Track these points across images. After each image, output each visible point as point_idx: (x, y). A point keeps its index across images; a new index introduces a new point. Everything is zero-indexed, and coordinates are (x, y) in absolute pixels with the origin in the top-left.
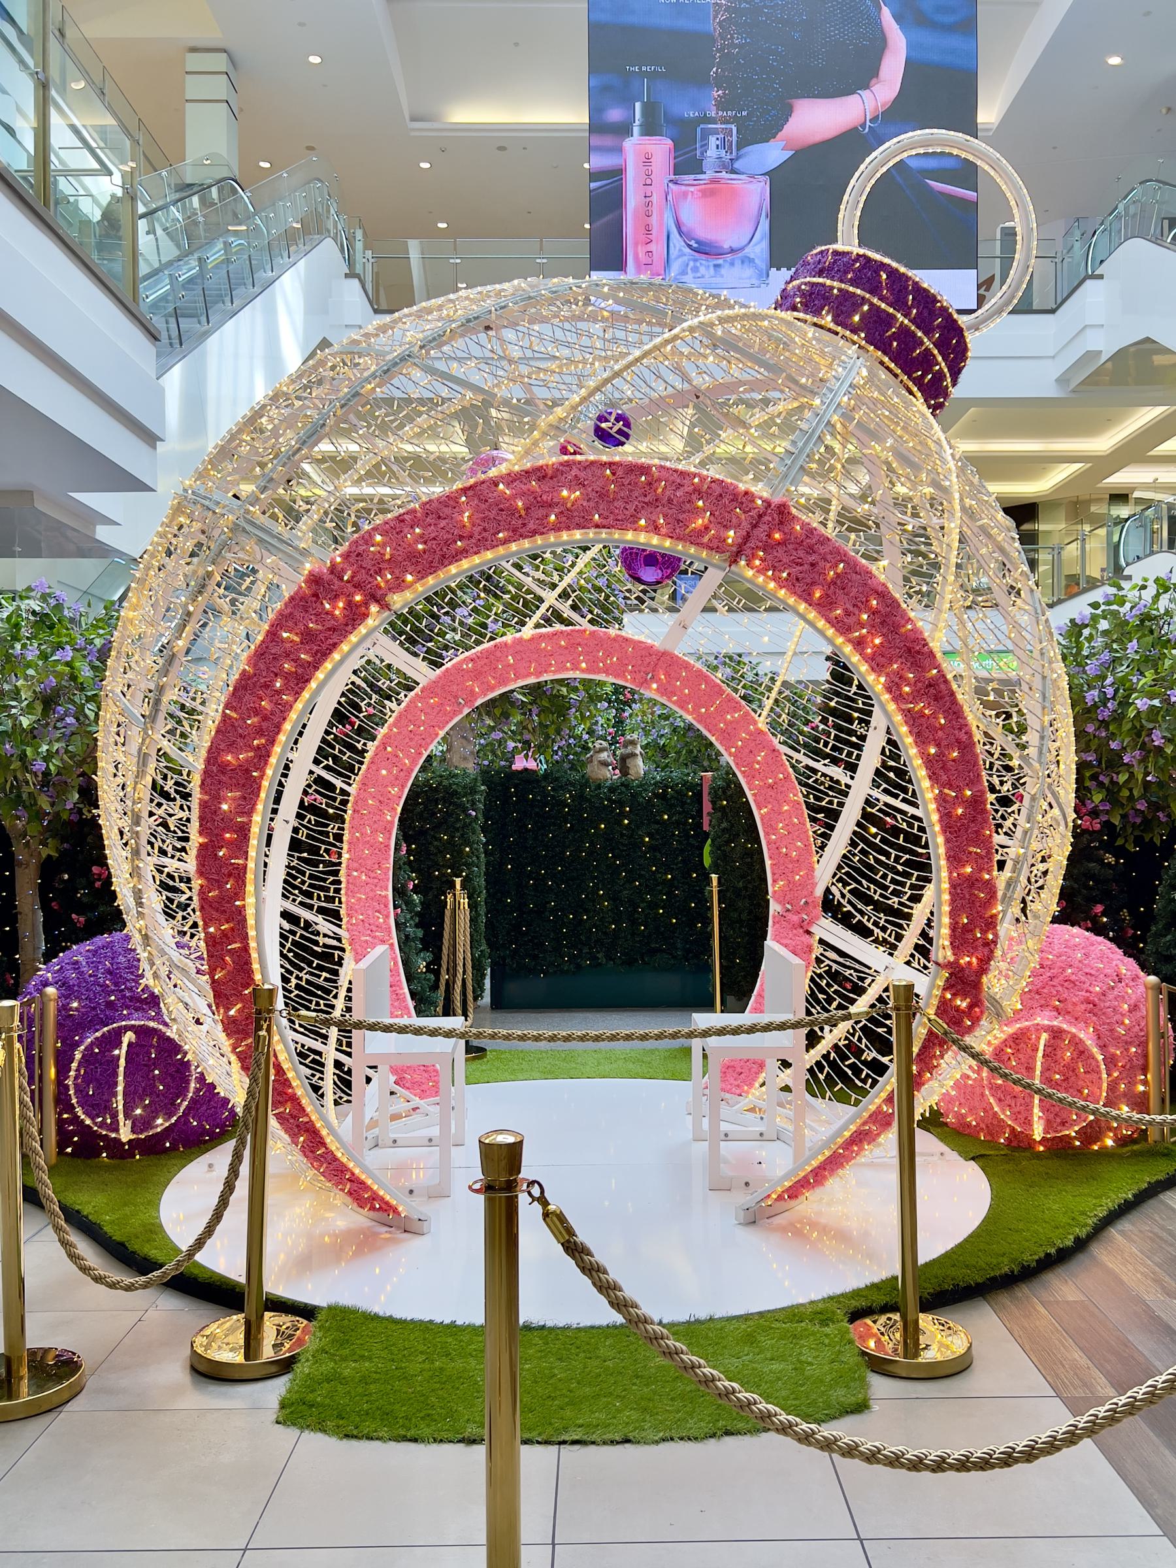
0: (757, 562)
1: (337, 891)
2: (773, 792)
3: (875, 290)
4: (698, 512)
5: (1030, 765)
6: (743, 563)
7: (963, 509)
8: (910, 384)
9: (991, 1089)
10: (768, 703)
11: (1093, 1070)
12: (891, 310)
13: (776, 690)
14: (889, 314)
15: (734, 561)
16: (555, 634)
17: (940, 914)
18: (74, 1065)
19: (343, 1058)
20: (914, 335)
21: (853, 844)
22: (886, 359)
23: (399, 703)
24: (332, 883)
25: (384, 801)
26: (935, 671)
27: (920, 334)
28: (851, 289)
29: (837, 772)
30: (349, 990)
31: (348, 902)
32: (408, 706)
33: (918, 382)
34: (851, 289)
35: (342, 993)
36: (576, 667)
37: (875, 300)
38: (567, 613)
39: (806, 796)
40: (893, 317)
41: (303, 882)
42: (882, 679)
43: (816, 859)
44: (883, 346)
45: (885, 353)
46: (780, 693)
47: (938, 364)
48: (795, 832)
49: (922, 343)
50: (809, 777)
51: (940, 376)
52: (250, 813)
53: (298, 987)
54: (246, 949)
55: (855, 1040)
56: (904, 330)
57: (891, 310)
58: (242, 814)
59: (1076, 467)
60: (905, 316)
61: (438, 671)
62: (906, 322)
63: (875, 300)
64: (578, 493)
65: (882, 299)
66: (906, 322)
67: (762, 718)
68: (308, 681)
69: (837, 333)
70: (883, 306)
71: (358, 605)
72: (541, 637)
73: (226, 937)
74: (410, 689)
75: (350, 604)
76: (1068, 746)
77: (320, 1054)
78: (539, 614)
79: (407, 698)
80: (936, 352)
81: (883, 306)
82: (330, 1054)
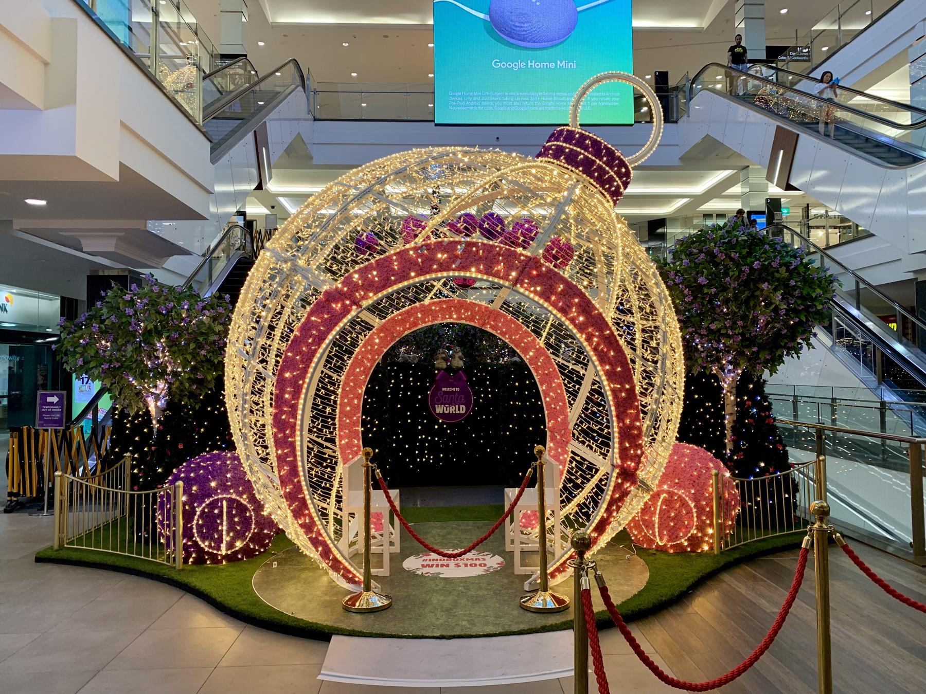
0: (525, 285)
1: (334, 429)
2: (548, 378)
3: (586, 148)
4: (498, 263)
5: (657, 372)
6: (519, 286)
7: (623, 254)
8: (603, 191)
9: (643, 522)
10: (545, 334)
11: (689, 512)
12: (594, 158)
13: (548, 327)
14: (593, 160)
15: (515, 284)
16: (440, 302)
17: (309, 494)
18: (196, 517)
19: (338, 512)
20: (605, 169)
21: (587, 403)
22: (592, 181)
23: (365, 336)
24: (332, 424)
25: (357, 385)
26: (608, 332)
27: (607, 168)
28: (575, 148)
29: (578, 368)
30: (341, 478)
31: (340, 434)
32: (369, 338)
33: (608, 190)
34: (575, 148)
35: (338, 480)
36: (451, 317)
37: (586, 154)
38: (446, 292)
39: (564, 380)
40: (594, 162)
41: (318, 425)
42: (584, 336)
43: (569, 410)
44: (590, 175)
45: (591, 178)
46: (550, 329)
47: (615, 181)
48: (560, 398)
49: (608, 173)
50: (565, 370)
51: (618, 187)
52: (298, 398)
53: (316, 476)
54: (295, 460)
55: (587, 503)
56: (600, 167)
57: (594, 158)
58: (294, 399)
59: (685, 200)
60: (600, 160)
61: (384, 321)
62: (601, 163)
63: (586, 154)
64: (446, 255)
65: (589, 152)
66: (601, 163)
67: (541, 341)
68: (324, 339)
69: (568, 169)
70: (590, 156)
71: (347, 305)
72: (434, 303)
73: (287, 455)
74: (370, 330)
75: (344, 305)
76: (680, 361)
77: (326, 509)
78: (432, 293)
79: (369, 334)
80: (615, 176)
81: (590, 156)
82: (332, 508)
